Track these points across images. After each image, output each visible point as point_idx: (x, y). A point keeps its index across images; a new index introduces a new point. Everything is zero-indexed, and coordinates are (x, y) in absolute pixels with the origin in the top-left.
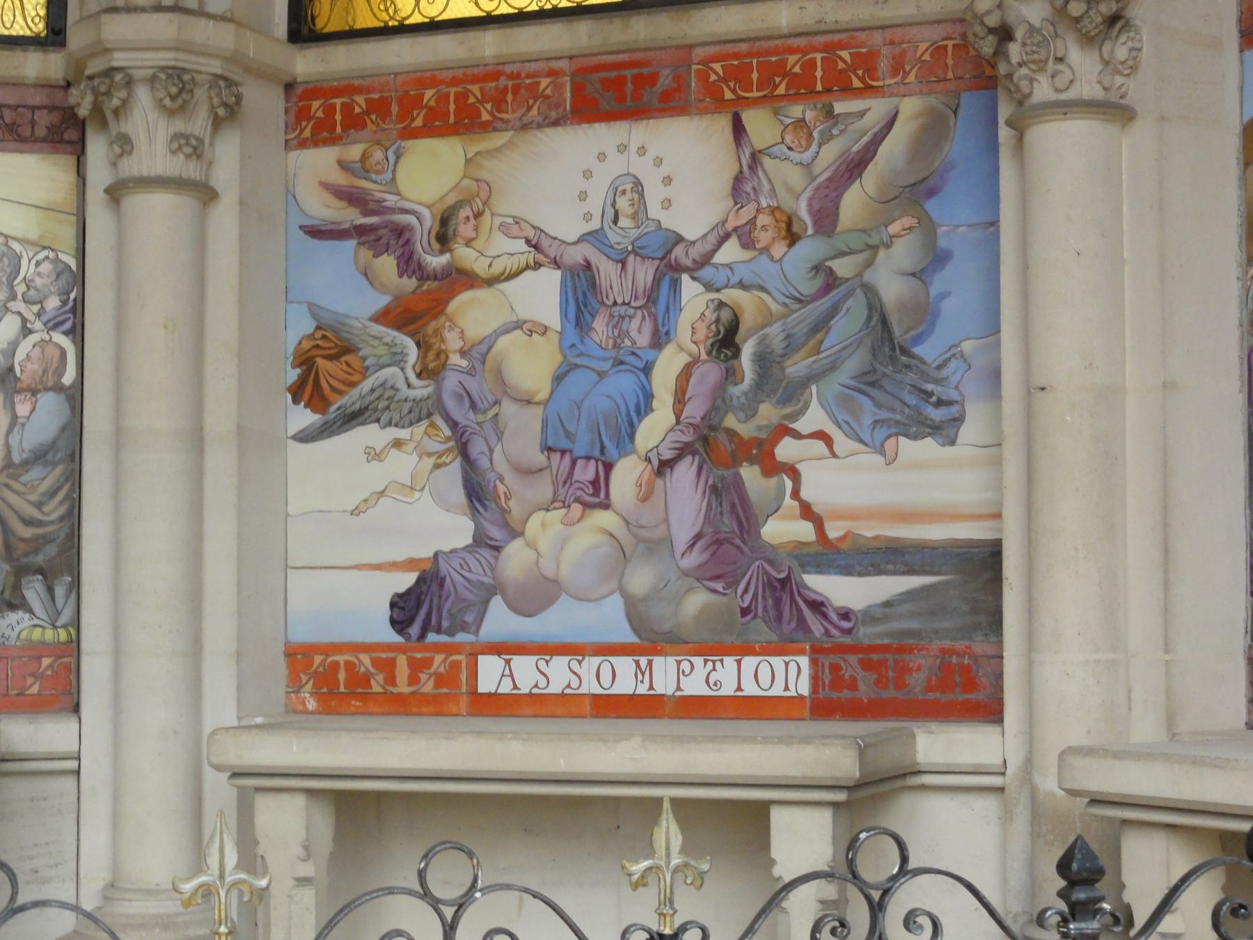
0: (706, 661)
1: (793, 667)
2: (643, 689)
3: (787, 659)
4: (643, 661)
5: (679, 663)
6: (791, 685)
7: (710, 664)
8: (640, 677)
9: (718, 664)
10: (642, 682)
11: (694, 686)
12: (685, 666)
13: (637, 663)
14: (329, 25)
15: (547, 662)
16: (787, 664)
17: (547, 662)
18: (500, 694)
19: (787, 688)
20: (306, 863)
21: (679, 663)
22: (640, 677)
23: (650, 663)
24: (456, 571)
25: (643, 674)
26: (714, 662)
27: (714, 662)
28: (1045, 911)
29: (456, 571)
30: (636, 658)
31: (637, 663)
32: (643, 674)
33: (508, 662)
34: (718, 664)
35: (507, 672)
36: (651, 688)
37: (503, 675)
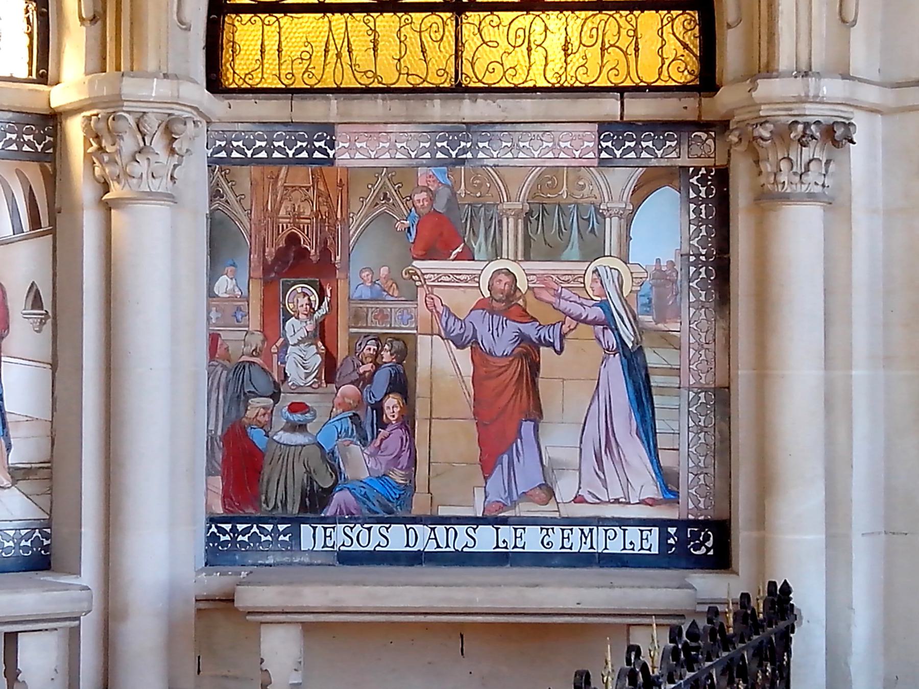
0: (542, 529)
1: (451, 531)
2: (585, 549)
3: (448, 527)
4: (586, 529)
5: (606, 531)
6: (451, 544)
7: (544, 531)
8: (584, 540)
9: (550, 531)
10: (585, 543)
11: (615, 547)
12: (611, 534)
13: (582, 530)
14: (598, 81)
15: (474, 529)
16: (447, 530)
17: (474, 529)
18: (582, 553)
19: (448, 546)
20: (840, 22)
21: (606, 531)
22: (584, 540)
23: (591, 530)
24: (276, 498)
25: (586, 538)
26: (547, 529)
27: (547, 529)
28: (36, 331)
29: (276, 498)
30: (581, 527)
31: (582, 530)
32: (586, 538)
33: (433, 529)
34: (550, 531)
35: (432, 536)
36: (592, 547)
37: (429, 539)
